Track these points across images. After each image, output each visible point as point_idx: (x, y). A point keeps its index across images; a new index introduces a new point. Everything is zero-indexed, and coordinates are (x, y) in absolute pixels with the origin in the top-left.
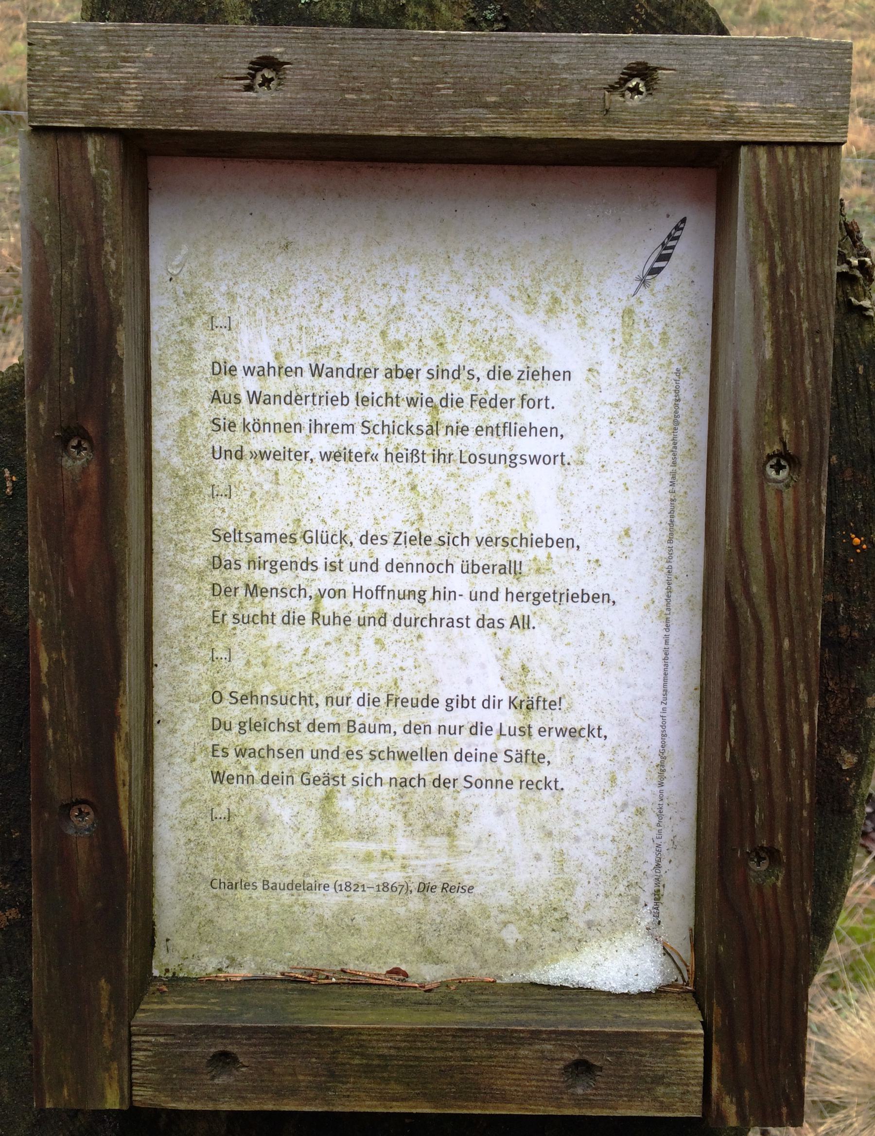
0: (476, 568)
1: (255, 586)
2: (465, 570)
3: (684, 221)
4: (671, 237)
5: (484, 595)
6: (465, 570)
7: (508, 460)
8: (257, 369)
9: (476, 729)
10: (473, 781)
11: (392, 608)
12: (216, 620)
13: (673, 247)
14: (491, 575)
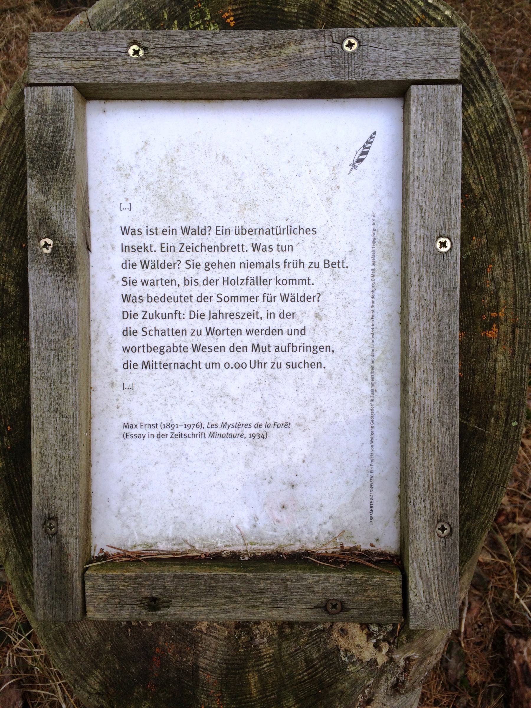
0: (244, 231)
1: (258, 345)
2: (237, 233)
3: (375, 133)
4: (368, 142)
5: (296, 331)
6: (237, 233)
7: (312, 349)
8: (149, 282)
9: (202, 299)
10: (223, 297)
11: (156, 357)
12: (218, 232)
13: (369, 148)
14: (217, 269)
